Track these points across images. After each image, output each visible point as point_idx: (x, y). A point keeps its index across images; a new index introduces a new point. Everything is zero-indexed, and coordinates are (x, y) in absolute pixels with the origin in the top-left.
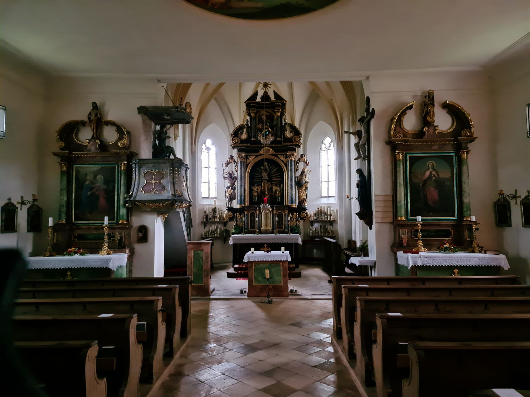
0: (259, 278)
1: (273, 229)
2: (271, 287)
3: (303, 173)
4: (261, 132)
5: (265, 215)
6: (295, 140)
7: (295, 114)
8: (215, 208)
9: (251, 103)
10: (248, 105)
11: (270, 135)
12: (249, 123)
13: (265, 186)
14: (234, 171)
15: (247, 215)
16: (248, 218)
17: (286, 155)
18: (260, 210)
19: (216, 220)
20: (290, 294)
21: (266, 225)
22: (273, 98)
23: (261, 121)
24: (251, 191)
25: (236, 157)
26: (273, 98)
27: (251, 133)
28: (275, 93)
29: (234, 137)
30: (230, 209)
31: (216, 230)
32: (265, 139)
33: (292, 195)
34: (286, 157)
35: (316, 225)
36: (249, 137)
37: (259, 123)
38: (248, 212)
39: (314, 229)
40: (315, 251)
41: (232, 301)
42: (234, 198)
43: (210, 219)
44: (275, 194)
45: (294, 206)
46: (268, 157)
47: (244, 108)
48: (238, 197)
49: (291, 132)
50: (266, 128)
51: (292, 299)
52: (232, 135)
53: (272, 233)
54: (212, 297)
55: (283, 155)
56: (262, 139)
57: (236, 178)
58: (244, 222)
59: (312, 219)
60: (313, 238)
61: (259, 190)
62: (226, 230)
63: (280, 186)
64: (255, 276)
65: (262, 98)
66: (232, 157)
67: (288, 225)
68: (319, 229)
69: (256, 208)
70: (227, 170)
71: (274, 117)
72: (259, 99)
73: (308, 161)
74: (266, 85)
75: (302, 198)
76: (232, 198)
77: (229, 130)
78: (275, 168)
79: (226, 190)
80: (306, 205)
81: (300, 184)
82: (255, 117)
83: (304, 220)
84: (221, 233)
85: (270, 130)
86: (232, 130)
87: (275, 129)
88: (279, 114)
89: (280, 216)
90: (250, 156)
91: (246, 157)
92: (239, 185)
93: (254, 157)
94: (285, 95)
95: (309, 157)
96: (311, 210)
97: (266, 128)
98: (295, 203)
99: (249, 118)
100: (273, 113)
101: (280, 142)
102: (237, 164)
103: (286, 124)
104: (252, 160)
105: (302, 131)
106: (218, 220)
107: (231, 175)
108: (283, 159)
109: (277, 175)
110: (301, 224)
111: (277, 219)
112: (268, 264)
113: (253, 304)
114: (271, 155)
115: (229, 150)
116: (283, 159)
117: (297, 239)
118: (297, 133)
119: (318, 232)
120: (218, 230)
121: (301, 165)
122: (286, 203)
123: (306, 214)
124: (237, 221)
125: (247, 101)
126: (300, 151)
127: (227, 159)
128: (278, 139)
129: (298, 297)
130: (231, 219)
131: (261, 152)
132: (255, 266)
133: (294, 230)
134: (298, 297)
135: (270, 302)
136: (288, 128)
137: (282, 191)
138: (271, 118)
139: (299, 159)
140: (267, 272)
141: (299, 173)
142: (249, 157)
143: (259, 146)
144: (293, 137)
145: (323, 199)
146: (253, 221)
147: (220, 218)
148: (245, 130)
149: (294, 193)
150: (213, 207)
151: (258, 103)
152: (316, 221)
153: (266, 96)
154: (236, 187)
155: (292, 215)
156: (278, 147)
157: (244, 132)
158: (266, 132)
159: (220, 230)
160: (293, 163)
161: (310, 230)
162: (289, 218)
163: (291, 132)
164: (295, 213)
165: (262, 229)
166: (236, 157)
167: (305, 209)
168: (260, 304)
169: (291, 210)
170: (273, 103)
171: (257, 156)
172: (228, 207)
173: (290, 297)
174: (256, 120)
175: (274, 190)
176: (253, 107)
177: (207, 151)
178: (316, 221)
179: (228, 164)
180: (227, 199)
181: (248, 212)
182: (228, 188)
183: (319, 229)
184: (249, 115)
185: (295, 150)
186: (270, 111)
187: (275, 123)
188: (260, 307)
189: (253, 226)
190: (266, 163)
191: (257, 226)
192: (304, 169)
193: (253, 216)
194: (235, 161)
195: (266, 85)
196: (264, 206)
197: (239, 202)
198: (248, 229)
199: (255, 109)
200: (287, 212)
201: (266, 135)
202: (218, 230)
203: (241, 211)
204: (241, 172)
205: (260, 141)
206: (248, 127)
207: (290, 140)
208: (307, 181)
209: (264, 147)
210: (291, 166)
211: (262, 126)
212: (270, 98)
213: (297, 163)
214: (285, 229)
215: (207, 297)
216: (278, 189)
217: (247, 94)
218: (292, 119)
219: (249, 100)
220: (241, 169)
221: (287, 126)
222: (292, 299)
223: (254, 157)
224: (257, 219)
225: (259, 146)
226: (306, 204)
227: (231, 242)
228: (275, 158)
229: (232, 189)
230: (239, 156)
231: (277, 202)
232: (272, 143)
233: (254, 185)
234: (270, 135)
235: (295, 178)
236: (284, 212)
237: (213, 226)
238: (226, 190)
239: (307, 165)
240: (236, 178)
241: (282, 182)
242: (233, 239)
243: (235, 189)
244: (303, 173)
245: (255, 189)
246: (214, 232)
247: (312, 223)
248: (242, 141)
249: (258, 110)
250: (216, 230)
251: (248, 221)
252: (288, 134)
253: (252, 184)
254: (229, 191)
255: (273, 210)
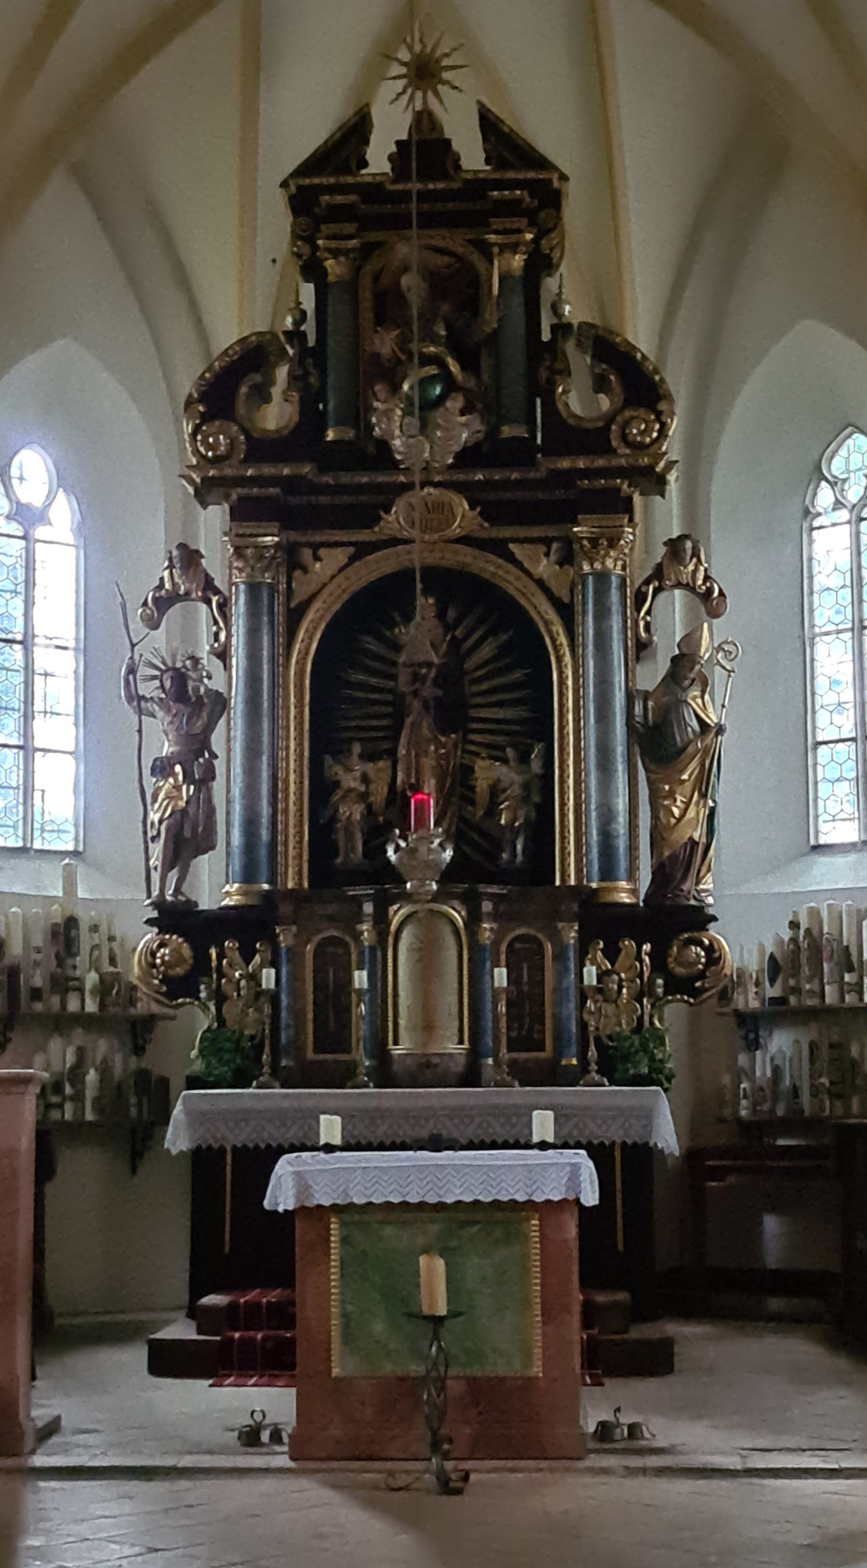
0: (379, 1327)
1: (475, 1054)
2: (455, 1387)
3: (684, 664)
4: (395, 388)
5: (421, 976)
6: (624, 438)
7: (624, 266)
8: (71, 922)
9: (330, 195)
10: (303, 201)
11: (455, 403)
12: (309, 328)
13: (422, 760)
14: (204, 651)
15: (295, 954)
16: (296, 977)
17: (568, 542)
18: (381, 920)
19: (73, 1005)
20: (592, 1445)
21: (427, 1026)
22: (472, 155)
23: (388, 306)
24: (322, 790)
25: (217, 558)
26: (472, 155)
27: (321, 395)
28: (490, 125)
29: (205, 418)
30: (174, 917)
31: (76, 1074)
32: (424, 427)
33: (607, 816)
34: (567, 559)
35: (781, 1043)
36: (311, 419)
37: (380, 320)
38: (302, 939)
39: (762, 1070)
40: (771, 1224)
41: (184, 1484)
42: (206, 844)
43: (36, 994)
44: (492, 811)
45: (622, 895)
46: (432, 559)
47: (276, 221)
48: (230, 833)
49: (600, 385)
50: (427, 360)
51: (605, 1471)
52: (189, 403)
53: (471, 1077)
54: (39, 1460)
55: (547, 542)
56: (392, 425)
57: (220, 703)
58: (274, 998)
59: (749, 1000)
60: (756, 1130)
61: (380, 792)
62: (142, 1075)
63: (524, 758)
64: (345, 1315)
65: (401, 155)
66: (189, 558)
67: (583, 1026)
68: (798, 1074)
69: (358, 902)
70: (158, 644)
71: (476, 284)
72: (378, 159)
73: (723, 581)
74: (424, 73)
75: (681, 835)
76: (186, 839)
77: (167, 376)
78: (493, 632)
79: (150, 781)
80: (709, 888)
81: (662, 742)
82: (351, 286)
83: (697, 993)
84: (112, 1095)
85: (454, 367)
86: (188, 378)
87: (486, 363)
88: (518, 261)
89: (524, 957)
90: (316, 547)
91: (291, 559)
92: (238, 747)
93: (340, 556)
94: (550, 129)
95: (724, 561)
96: (743, 937)
97: (427, 360)
98: (632, 875)
99: (308, 294)
100: (476, 259)
101: (521, 453)
102: (223, 607)
103: (562, 329)
104: (332, 575)
105: (678, 380)
106: (91, 1006)
107: (180, 678)
108: (544, 567)
109: (502, 681)
110: (672, 1018)
111: (501, 976)
112: (434, 1228)
113: (328, 1495)
114: (464, 540)
115: (169, 513)
116: (544, 567)
117: (648, 1117)
118: (638, 385)
119: (795, 1091)
120: (92, 1076)
121: (672, 613)
122: (568, 871)
123: (710, 950)
124: (220, 998)
125: (299, 172)
126: (663, 515)
127: (156, 570)
128: (507, 431)
129: (653, 1461)
130: (178, 987)
131: (395, 520)
132: (345, 1240)
133: (621, 1060)
134: (653, 1461)
135: (448, 1487)
136: (579, 361)
137: (541, 792)
138: (458, 288)
139: (658, 573)
140: (434, 1270)
141: (651, 675)
142: (307, 554)
143: (381, 478)
144: (610, 419)
145: (823, 861)
146: (334, 998)
147: (104, 988)
148: (282, 373)
149: (621, 804)
150: (57, 914)
151: (373, 191)
152: (780, 1012)
153: (426, 148)
154: (219, 765)
155: (612, 953)
156: (506, 484)
157: (277, 392)
158: (425, 383)
159: (105, 1071)
160: (614, 596)
161: (738, 1075)
162: (590, 974)
163: (600, 385)
164: (628, 944)
165: (397, 1051)
166: (217, 558)
167: (700, 919)
168: (385, 1498)
169: (605, 924)
170: (478, 186)
171: (362, 550)
172: (159, 905)
173: (593, 1461)
174: (355, 303)
175: (482, 784)
176: (336, 214)
177: (14, 528)
178: (780, 1012)
179: (164, 602)
180: (157, 850)
181: (302, 939)
182: (162, 768)
183: (798, 1074)
184: (312, 269)
185: (627, 507)
186: (456, 241)
187: (490, 319)
188: (370, 1504)
189: (333, 1030)
190: (425, 605)
191: (360, 1030)
192: (691, 640)
193: (333, 962)
194: (209, 586)
195: (424, 73)
196: (412, 852)
197: (237, 864)
198: (297, 1047)
199: (350, 228)
200: (571, 935)
201: (430, 405)
202: (92, 1076)
203: (248, 925)
204: (253, 656)
205: (384, 446)
206: (304, 351)
207: (593, 438)
208: (712, 717)
209: (407, 487)
210: (602, 614)
211: (403, 342)
212: (457, 159)
213: (640, 598)
214: (559, 1052)
215: (10, 1462)
216: (509, 775)
217: (301, 125)
218: (608, 285)
219: (313, 165)
220: (253, 634)
221: (570, 347)
222: (605, 1471)
223: (340, 556)
224: (360, 978)
225: (381, 478)
226: (708, 883)
227: (177, 1138)
228: (487, 566)
229: (188, 777)
230: (239, 551)
231: (507, 866)
232: (467, 457)
233: (340, 752)
234: (455, 403)
235: (630, 697)
236: (556, 937)
237: (55, 1044)
238: (150, 781)
239: (714, 613)
240: (220, 703)
241: (535, 727)
242: (195, 1117)
243: (210, 774)
244: (684, 664)
245: (350, 781)
246: (57, 1087)
247: (751, 1028)
248: (261, 448)
249: (373, 236)
250: (76, 1074)
251: (296, 994)
252: (580, 399)
253: (326, 741)
254: (169, 795)
255: (473, 920)
